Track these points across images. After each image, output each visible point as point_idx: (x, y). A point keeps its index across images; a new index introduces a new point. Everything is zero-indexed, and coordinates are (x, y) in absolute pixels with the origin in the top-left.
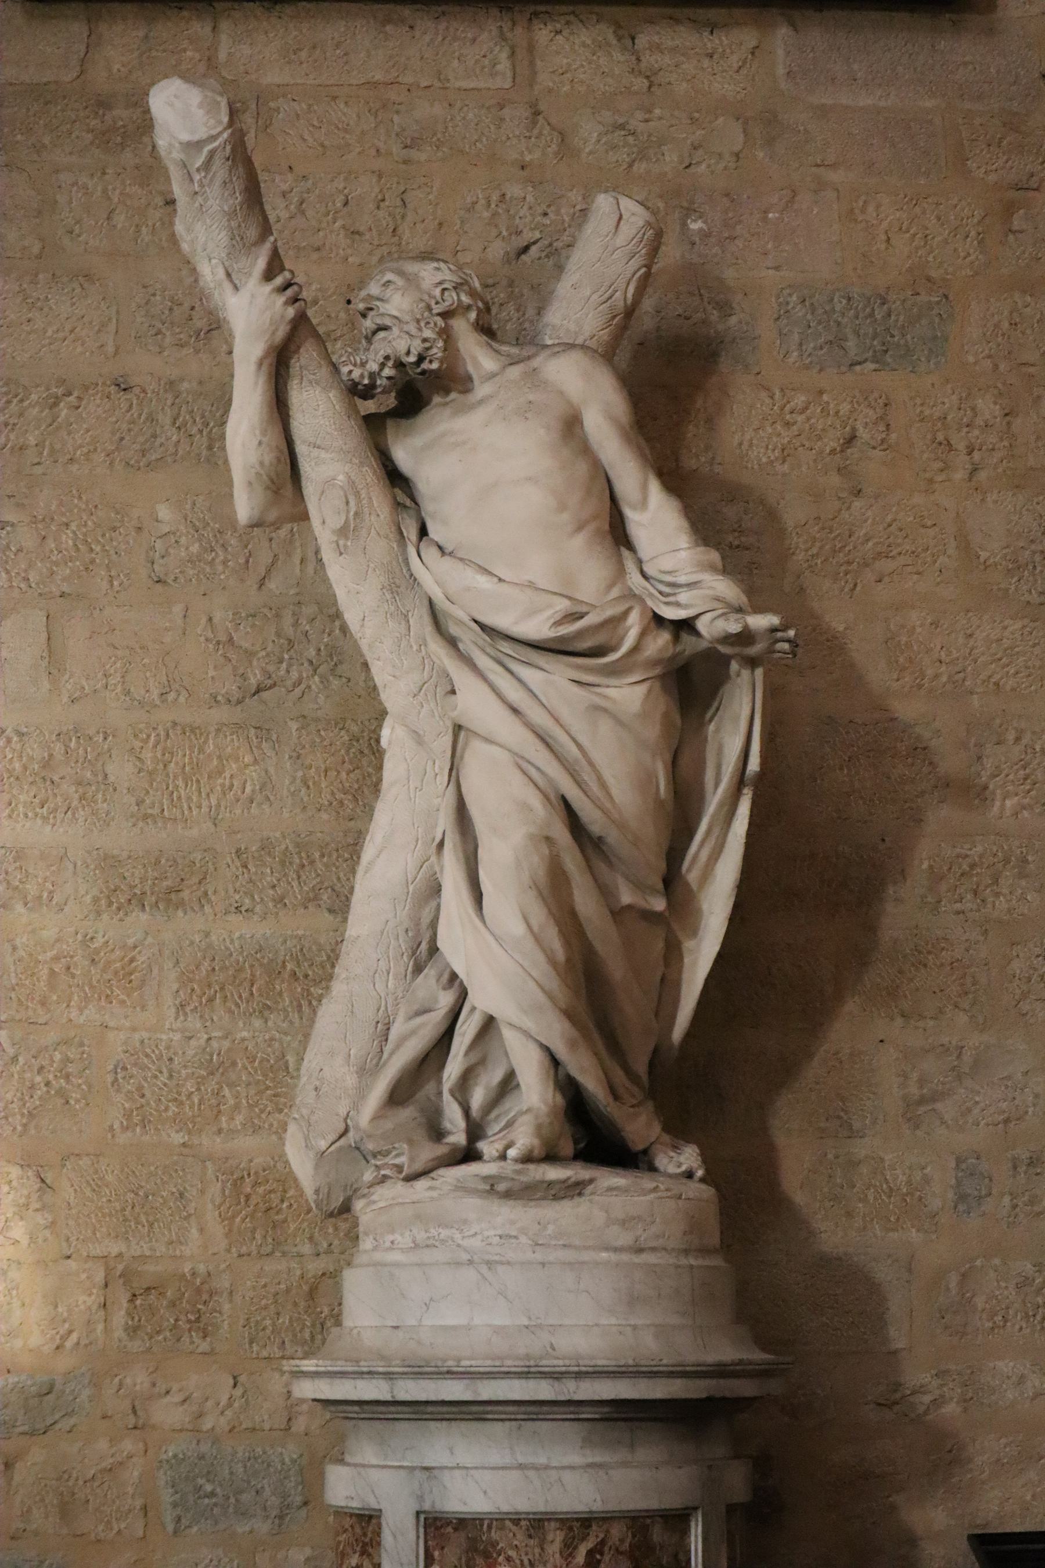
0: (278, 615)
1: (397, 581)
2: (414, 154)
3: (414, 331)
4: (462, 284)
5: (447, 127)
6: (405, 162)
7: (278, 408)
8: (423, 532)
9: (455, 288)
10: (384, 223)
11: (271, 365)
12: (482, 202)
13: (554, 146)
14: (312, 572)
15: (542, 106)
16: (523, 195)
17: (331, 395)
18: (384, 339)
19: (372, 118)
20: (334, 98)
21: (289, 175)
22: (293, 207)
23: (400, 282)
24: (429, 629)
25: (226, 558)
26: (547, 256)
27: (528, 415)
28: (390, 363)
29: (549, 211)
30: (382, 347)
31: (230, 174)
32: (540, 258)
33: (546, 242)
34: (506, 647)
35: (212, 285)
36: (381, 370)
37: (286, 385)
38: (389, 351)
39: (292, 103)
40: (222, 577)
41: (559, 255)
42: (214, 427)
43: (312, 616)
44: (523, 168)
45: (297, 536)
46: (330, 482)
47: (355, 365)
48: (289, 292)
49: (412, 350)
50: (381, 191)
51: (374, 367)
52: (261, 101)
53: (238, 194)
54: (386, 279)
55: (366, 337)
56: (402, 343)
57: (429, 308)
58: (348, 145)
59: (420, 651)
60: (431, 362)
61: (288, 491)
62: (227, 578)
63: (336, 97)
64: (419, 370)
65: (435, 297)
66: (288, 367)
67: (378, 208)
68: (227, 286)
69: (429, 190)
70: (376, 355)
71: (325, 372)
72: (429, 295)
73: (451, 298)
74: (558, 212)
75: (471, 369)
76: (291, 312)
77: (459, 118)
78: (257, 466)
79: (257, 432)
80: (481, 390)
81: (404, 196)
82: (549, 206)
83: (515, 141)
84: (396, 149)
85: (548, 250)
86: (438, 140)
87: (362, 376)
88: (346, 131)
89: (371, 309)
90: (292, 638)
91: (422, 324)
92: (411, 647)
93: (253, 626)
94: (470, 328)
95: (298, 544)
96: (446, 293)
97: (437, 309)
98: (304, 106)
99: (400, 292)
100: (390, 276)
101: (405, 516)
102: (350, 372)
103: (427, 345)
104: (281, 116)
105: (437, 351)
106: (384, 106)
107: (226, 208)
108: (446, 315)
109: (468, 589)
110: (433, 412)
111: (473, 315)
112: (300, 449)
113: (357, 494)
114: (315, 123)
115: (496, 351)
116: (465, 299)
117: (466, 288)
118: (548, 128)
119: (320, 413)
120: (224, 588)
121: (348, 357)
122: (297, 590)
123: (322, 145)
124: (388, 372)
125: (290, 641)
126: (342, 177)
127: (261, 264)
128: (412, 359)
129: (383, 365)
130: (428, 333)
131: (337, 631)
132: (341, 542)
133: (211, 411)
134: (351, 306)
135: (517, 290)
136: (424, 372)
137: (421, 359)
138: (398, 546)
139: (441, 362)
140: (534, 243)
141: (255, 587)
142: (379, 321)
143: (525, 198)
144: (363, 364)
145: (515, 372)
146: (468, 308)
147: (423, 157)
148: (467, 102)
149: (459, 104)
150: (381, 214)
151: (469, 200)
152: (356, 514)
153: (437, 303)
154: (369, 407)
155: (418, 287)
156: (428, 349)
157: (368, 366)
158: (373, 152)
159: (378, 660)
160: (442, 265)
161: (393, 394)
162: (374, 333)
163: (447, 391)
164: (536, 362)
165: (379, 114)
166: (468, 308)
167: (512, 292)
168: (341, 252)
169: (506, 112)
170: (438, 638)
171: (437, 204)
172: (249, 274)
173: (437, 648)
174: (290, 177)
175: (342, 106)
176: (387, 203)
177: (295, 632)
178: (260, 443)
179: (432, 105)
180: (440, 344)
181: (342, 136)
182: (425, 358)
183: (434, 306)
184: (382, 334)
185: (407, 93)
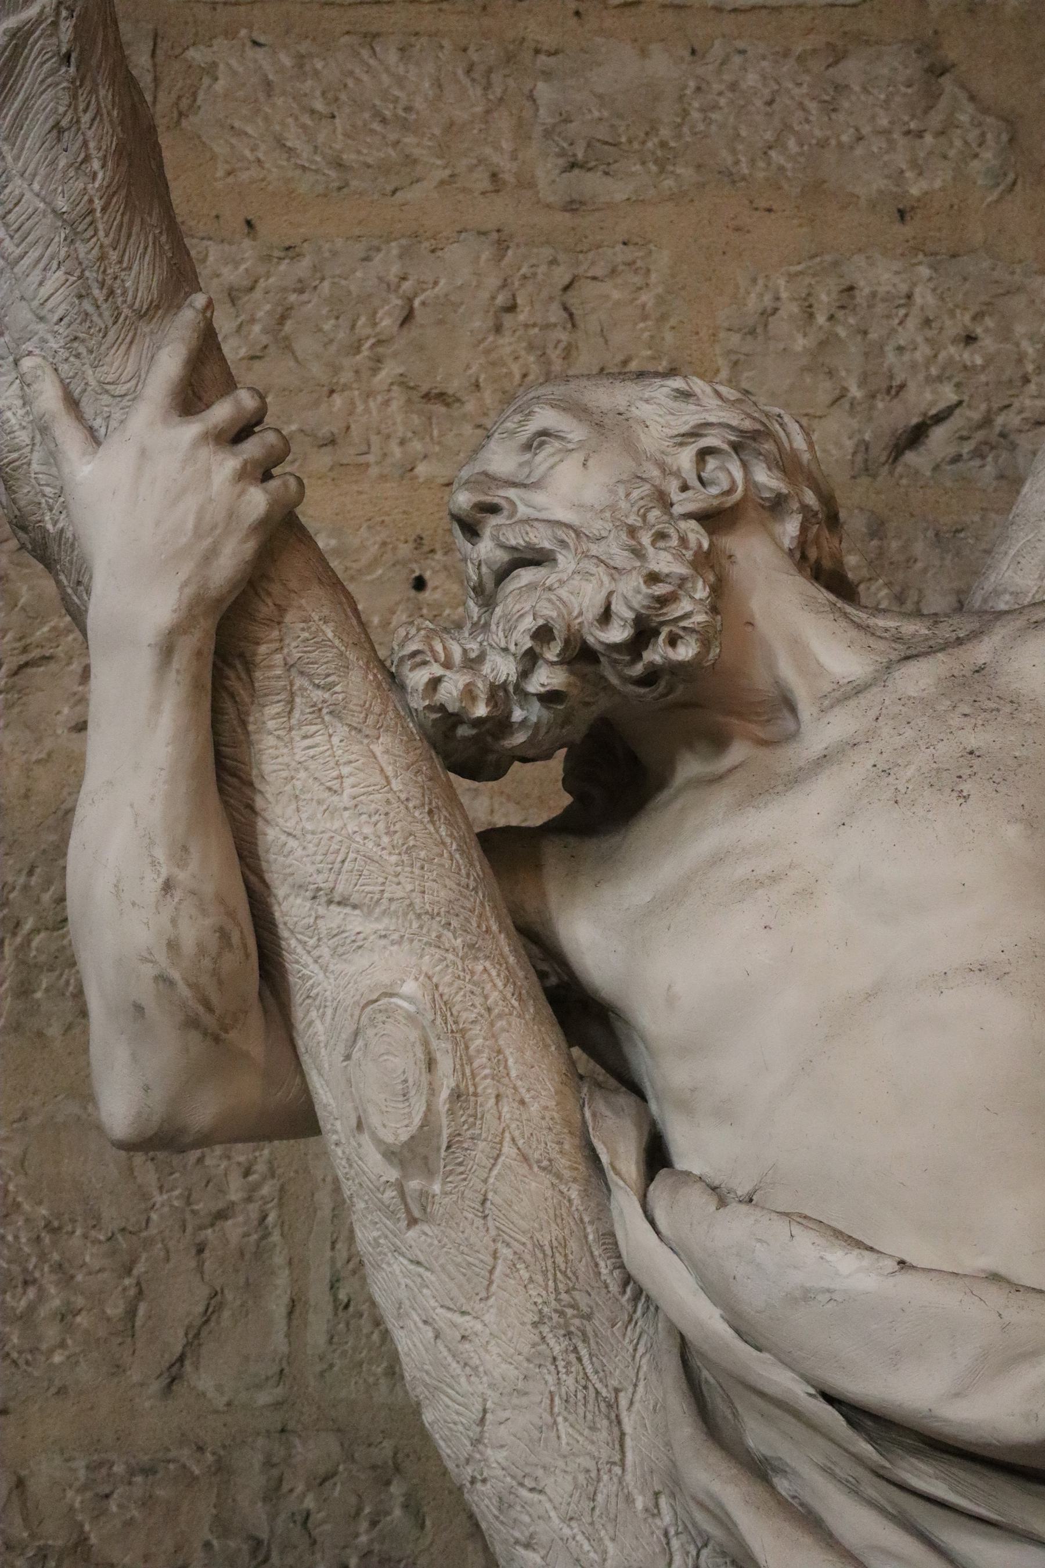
0: (221, 1468)
1: (583, 1301)
2: (592, 183)
3: (621, 558)
4: (755, 435)
5: (685, 113)
6: (573, 206)
7: (221, 791)
8: (656, 1156)
9: (736, 447)
10: (516, 369)
11: (199, 654)
12: (791, 308)
13: (987, 155)
14: (322, 1340)
15: (952, 52)
16: (904, 288)
17: (378, 749)
18: (532, 587)
19: (475, 92)
20: (371, 38)
21: (247, 243)
22: (257, 328)
23: (575, 431)
24: (685, 1429)
25: (68, 1303)
26: (978, 453)
27: (966, 787)
28: (552, 653)
29: (979, 330)
30: (525, 603)
31: (73, 105)
32: (957, 459)
33: (976, 416)
34: (926, 1477)
35: (23, 437)
36: (525, 674)
37: (247, 740)
38: (548, 612)
39: (250, 52)
40: (57, 1358)
41: (1013, 447)
42: (36, 931)
43: (322, 1470)
44: (902, 214)
45: (276, 1237)
46: (377, 1001)
47: (447, 665)
48: (252, 448)
49: (618, 607)
50: (504, 285)
51: (505, 668)
52: (163, 46)
53: (96, 165)
54: (533, 426)
55: (479, 590)
56: (584, 593)
57: (664, 501)
58: (410, 161)
59: (653, 1511)
60: (673, 641)
61: (252, 1039)
62: (72, 1361)
63: (376, 35)
64: (638, 669)
65: (677, 474)
66: (249, 666)
67: (498, 329)
68: (69, 436)
69: (637, 280)
70: (508, 633)
71: (357, 685)
72: (662, 467)
73: (728, 475)
74: (1005, 334)
75: (788, 671)
76: (257, 501)
77: (716, 87)
78: (162, 957)
79: (160, 853)
80: (821, 731)
81: (573, 299)
82: (978, 317)
83: (877, 144)
84: (546, 171)
85: (980, 435)
86: (663, 145)
87: (469, 692)
88: (405, 126)
89: (493, 509)
90: (265, 1536)
91: (646, 539)
92: (629, 1499)
93: (147, 1502)
94: (787, 564)
95: (279, 1259)
96: (712, 463)
97: (684, 502)
98: (286, 61)
99: (578, 457)
100: (545, 418)
101: (601, 1106)
102: (435, 683)
103: (660, 589)
104: (220, 86)
105: (691, 607)
106: (510, 58)
107: (62, 204)
108: (713, 519)
109: (807, 1296)
110: (677, 805)
111: (790, 528)
112: (291, 910)
113: (459, 1036)
114: (319, 105)
115: (859, 626)
116: (765, 477)
117: (768, 446)
118: (970, 108)
119: (346, 799)
120: (62, 1391)
121: (428, 639)
122: (279, 1391)
123: (339, 165)
124: (546, 678)
125: (259, 1543)
126: (394, 249)
127: (169, 363)
128: (618, 634)
129: (530, 660)
130: (663, 562)
131: (397, 1512)
132: (414, 1184)
133: (26, 888)
134: (427, 595)
135: (895, 545)
136: (651, 677)
137: (644, 632)
138: (585, 1194)
139: (706, 644)
140: (939, 418)
141: (155, 1387)
142: (514, 539)
143: (909, 296)
144: (473, 663)
145: (920, 678)
146: (777, 506)
147: (619, 191)
148: (740, 44)
149: (718, 49)
150: (507, 344)
151: (753, 304)
152: (457, 1095)
153: (685, 488)
154: (490, 805)
155: (630, 447)
156: (663, 601)
157: (486, 669)
158: (480, 181)
159: (527, 1546)
160: (698, 385)
161: (556, 765)
162: (503, 575)
163: (719, 742)
164: (981, 652)
165: (496, 78)
166: (777, 506)
167: (881, 553)
168: (397, 451)
169: (852, 69)
170: (715, 1457)
171: (663, 318)
172: (134, 396)
173: (713, 1478)
174: (248, 250)
175: (392, 57)
176: (522, 317)
177: (273, 1517)
178: (168, 886)
179: (644, 53)
180: (701, 592)
181: (392, 137)
182: (656, 633)
183: (675, 496)
184: (526, 576)
185: (573, 22)
